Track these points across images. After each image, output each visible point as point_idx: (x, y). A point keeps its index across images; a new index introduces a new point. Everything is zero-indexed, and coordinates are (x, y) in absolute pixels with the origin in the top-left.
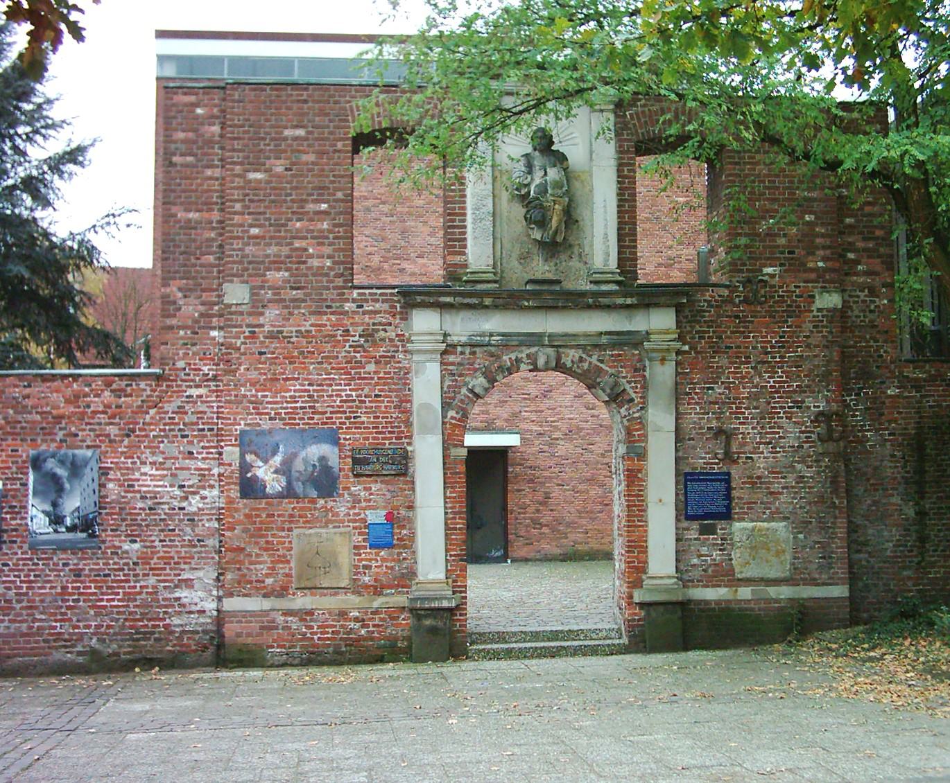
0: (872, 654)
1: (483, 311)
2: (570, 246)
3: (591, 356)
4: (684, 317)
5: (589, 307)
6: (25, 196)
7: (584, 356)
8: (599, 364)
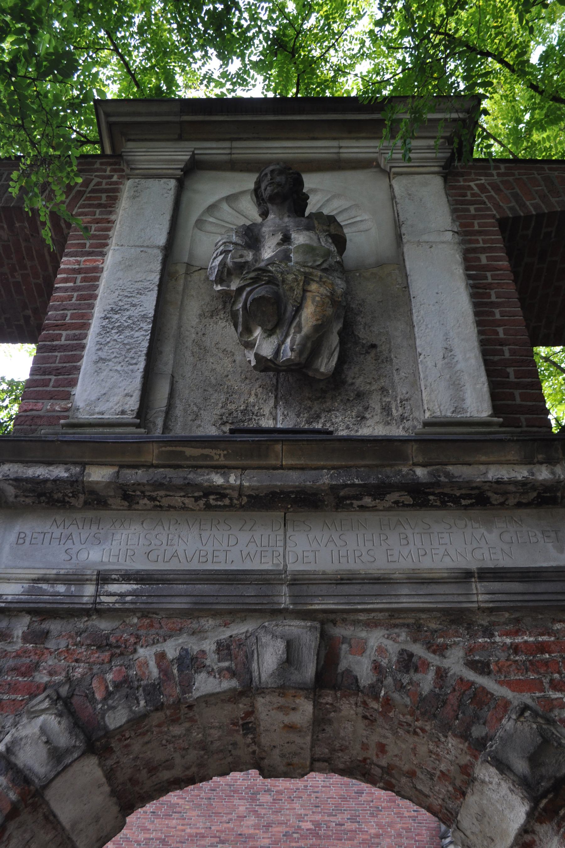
0: (219, 503)
1: (90, 514)
2: (360, 395)
3: (441, 650)
7: (418, 650)
8: (471, 676)
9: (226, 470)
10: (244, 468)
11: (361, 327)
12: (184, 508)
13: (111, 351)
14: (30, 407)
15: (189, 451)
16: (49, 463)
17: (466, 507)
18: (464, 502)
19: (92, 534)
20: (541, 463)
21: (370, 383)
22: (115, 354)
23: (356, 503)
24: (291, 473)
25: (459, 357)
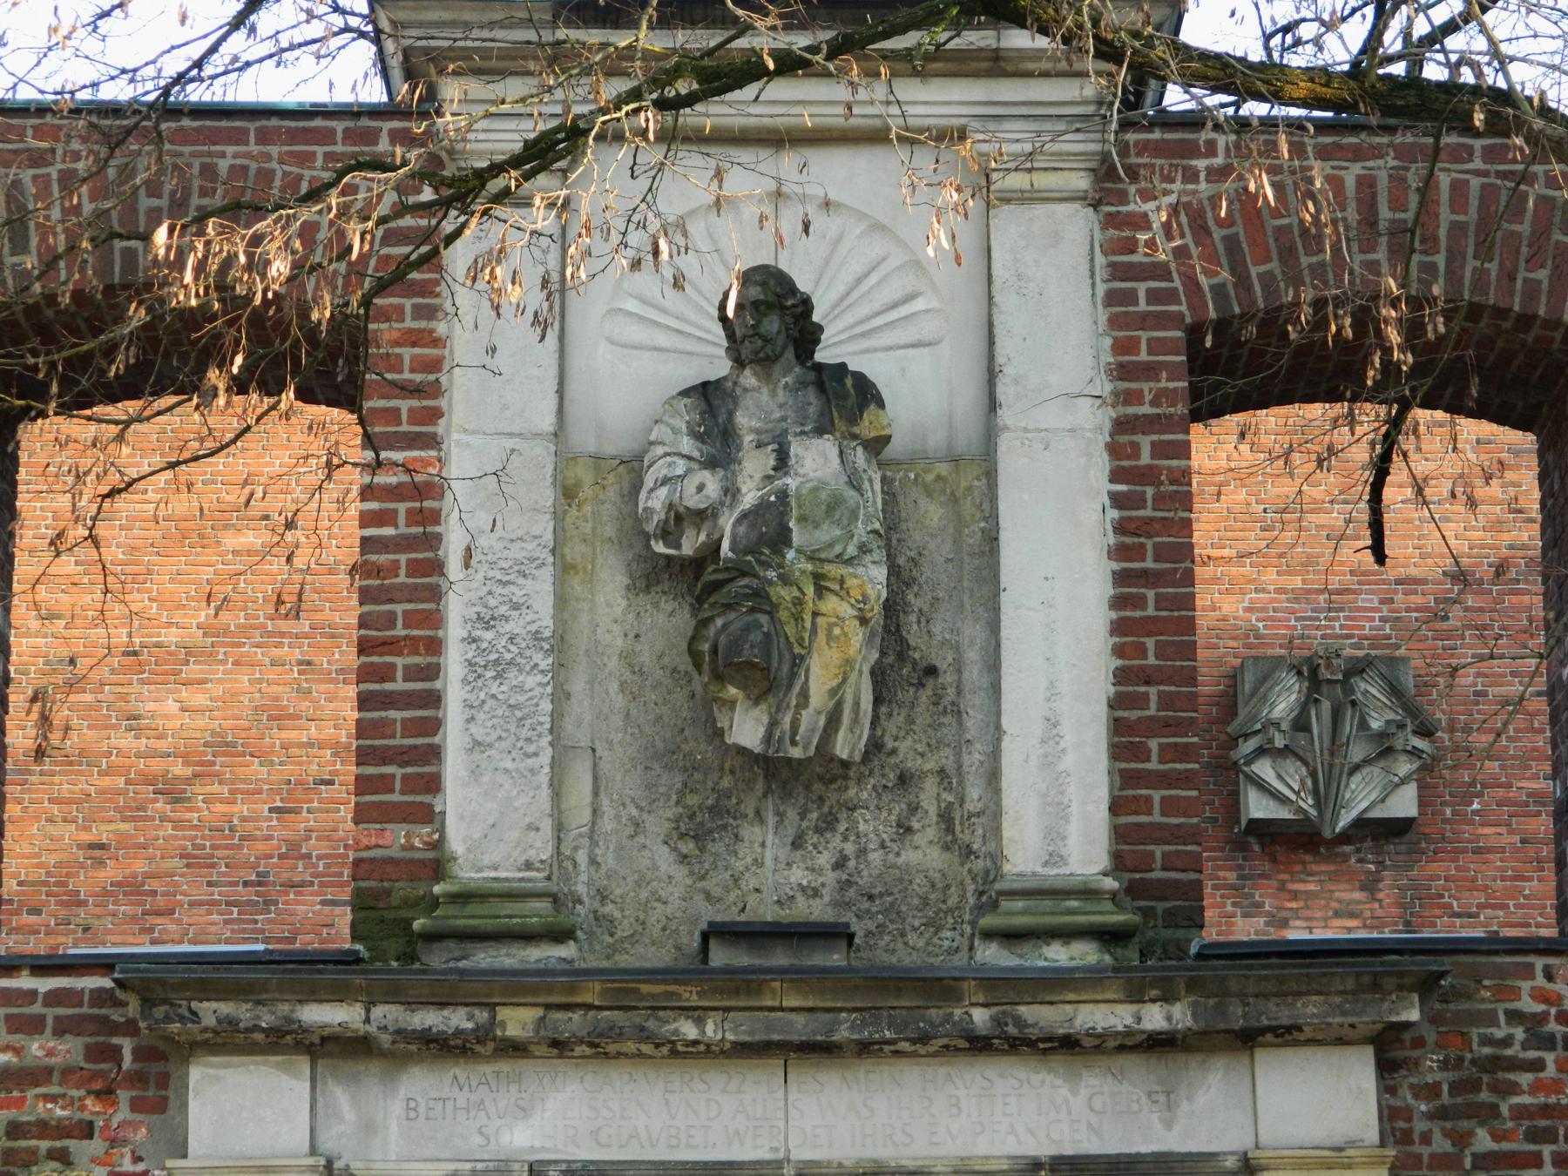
1: (504, 1066)
4: (1418, 1091)
5: (979, 1045)
6: (1477, 123)
9: (700, 1013)
10: (727, 1010)
11: (913, 618)
12: (640, 1055)
13: (490, 724)
14: (373, 841)
15: (645, 988)
16: (443, 1005)
17: (1045, 1051)
18: (1041, 1046)
19: (513, 1101)
20: (1153, 1001)
21: (922, 755)
22: (499, 732)
23: (887, 1048)
24: (793, 1016)
25: (1068, 740)
